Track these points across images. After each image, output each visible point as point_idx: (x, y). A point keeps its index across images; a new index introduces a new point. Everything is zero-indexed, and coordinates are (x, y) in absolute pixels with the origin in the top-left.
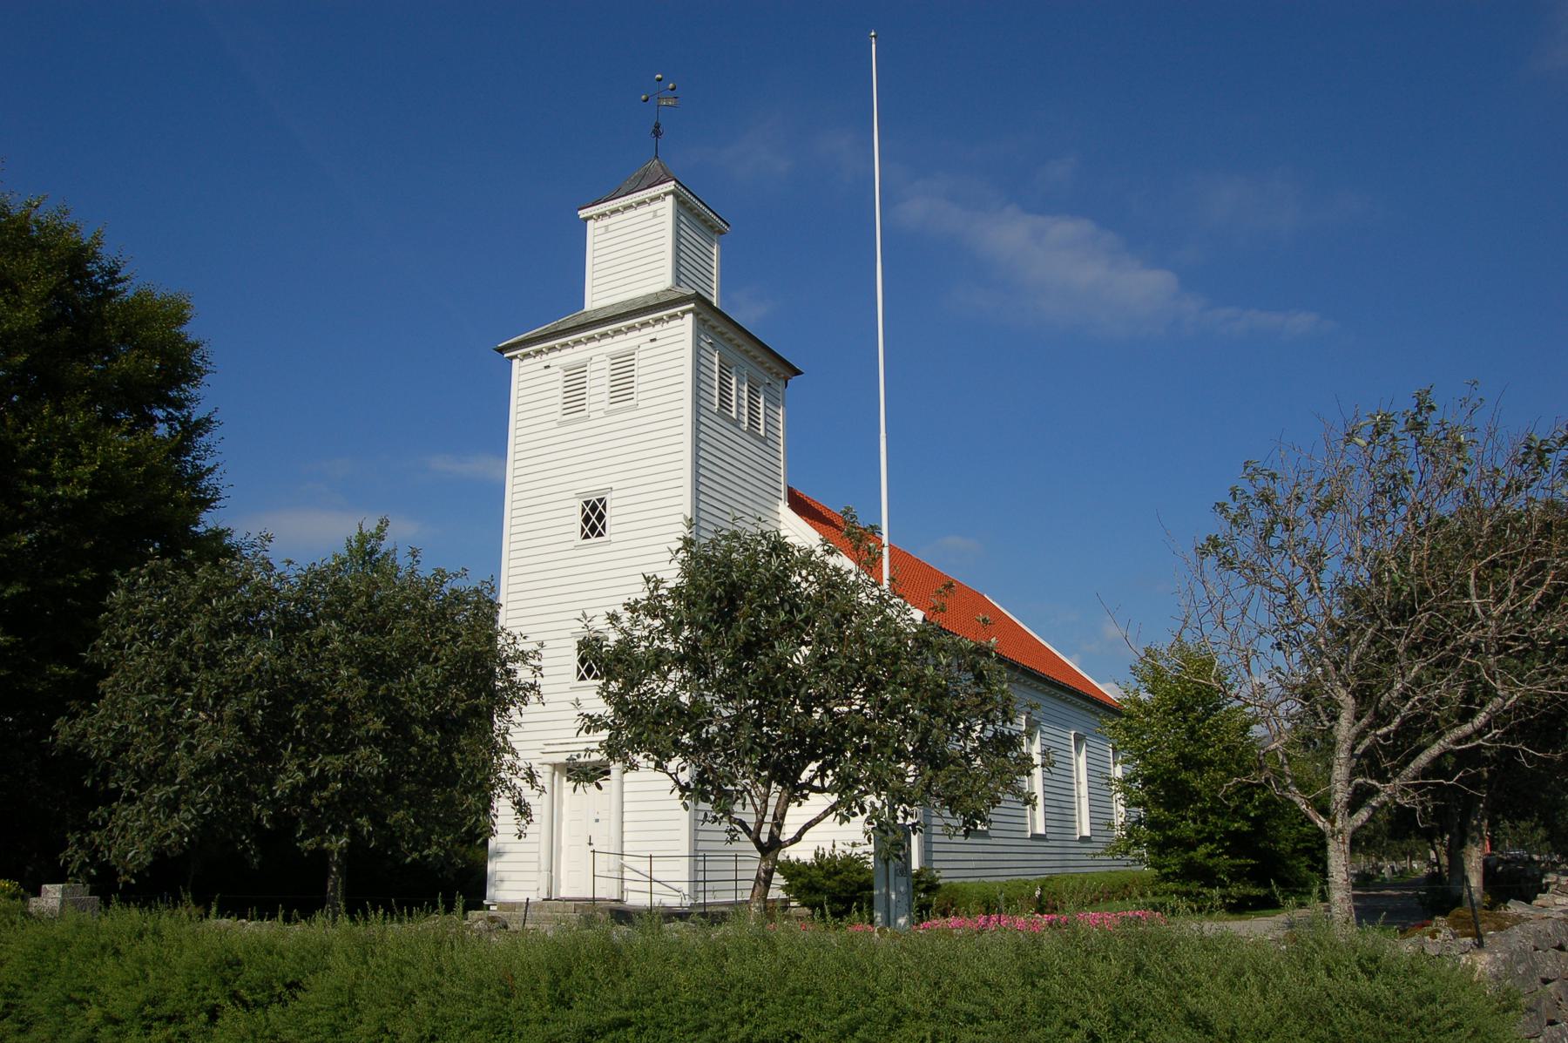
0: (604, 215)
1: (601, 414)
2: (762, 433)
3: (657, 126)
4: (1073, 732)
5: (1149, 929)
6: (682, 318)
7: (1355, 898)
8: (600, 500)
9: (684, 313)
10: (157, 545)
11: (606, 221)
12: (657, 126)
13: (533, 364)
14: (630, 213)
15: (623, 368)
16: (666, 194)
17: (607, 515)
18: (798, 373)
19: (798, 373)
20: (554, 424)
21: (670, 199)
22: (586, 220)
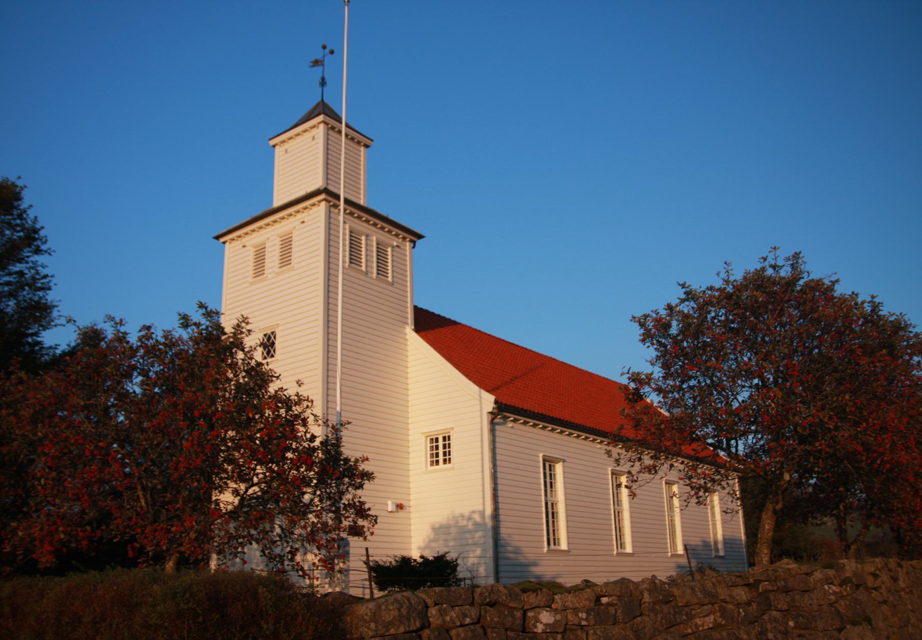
0: (284, 142)
1: (273, 275)
2: (390, 279)
3: (323, 79)
4: (541, 455)
5: (39, 488)
6: (319, 205)
7: (409, 494)
8: (272, 333)
9: (320, 201)
10: (287, 442)
11: (286, 146)
12: (323, 79)
13: (237, 244)
14: (299, 139)
15: (287, 244)
16: (319, 123)
17: (276, 343)
18: (420, 237)
19: (420, 237)
20: (247, 285)
21: (322, 126)
22: (274, 146)
